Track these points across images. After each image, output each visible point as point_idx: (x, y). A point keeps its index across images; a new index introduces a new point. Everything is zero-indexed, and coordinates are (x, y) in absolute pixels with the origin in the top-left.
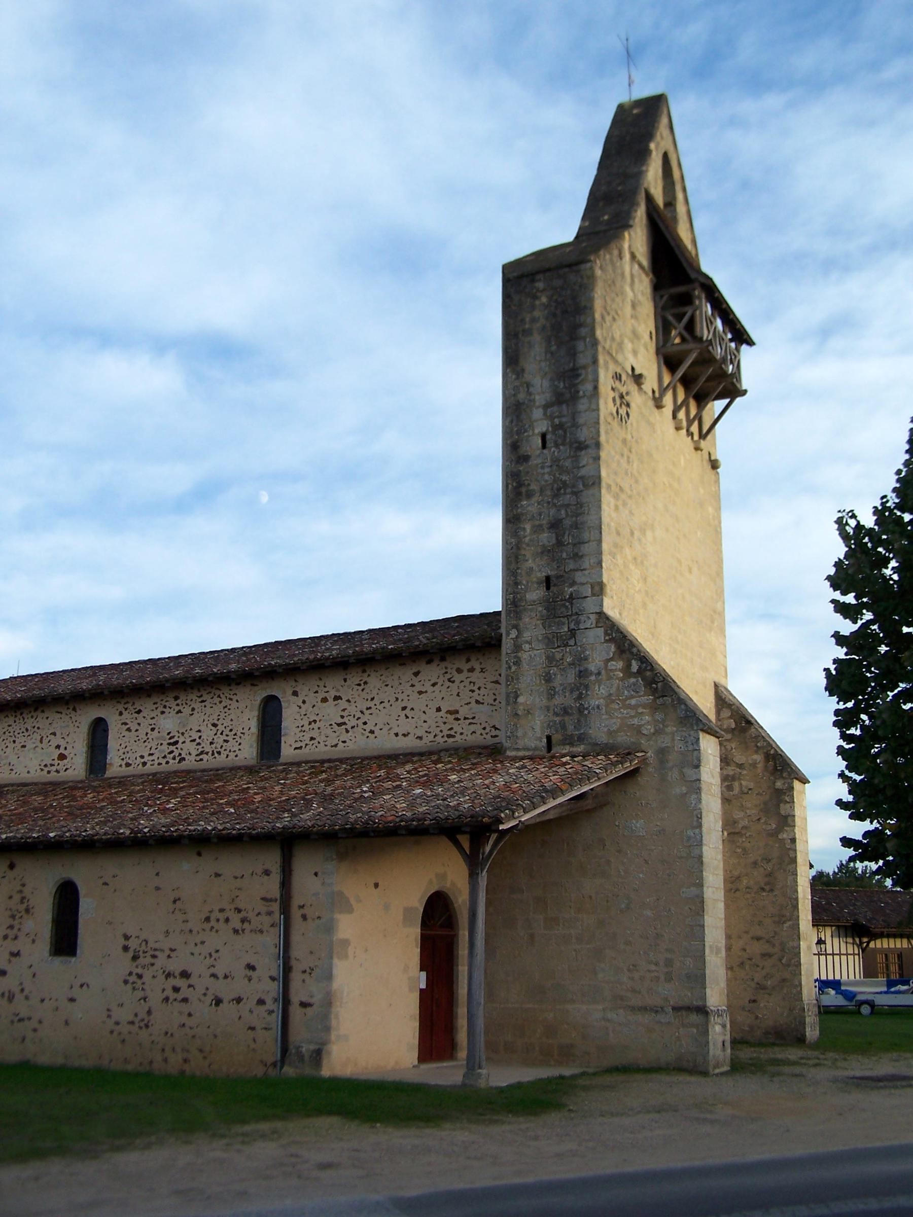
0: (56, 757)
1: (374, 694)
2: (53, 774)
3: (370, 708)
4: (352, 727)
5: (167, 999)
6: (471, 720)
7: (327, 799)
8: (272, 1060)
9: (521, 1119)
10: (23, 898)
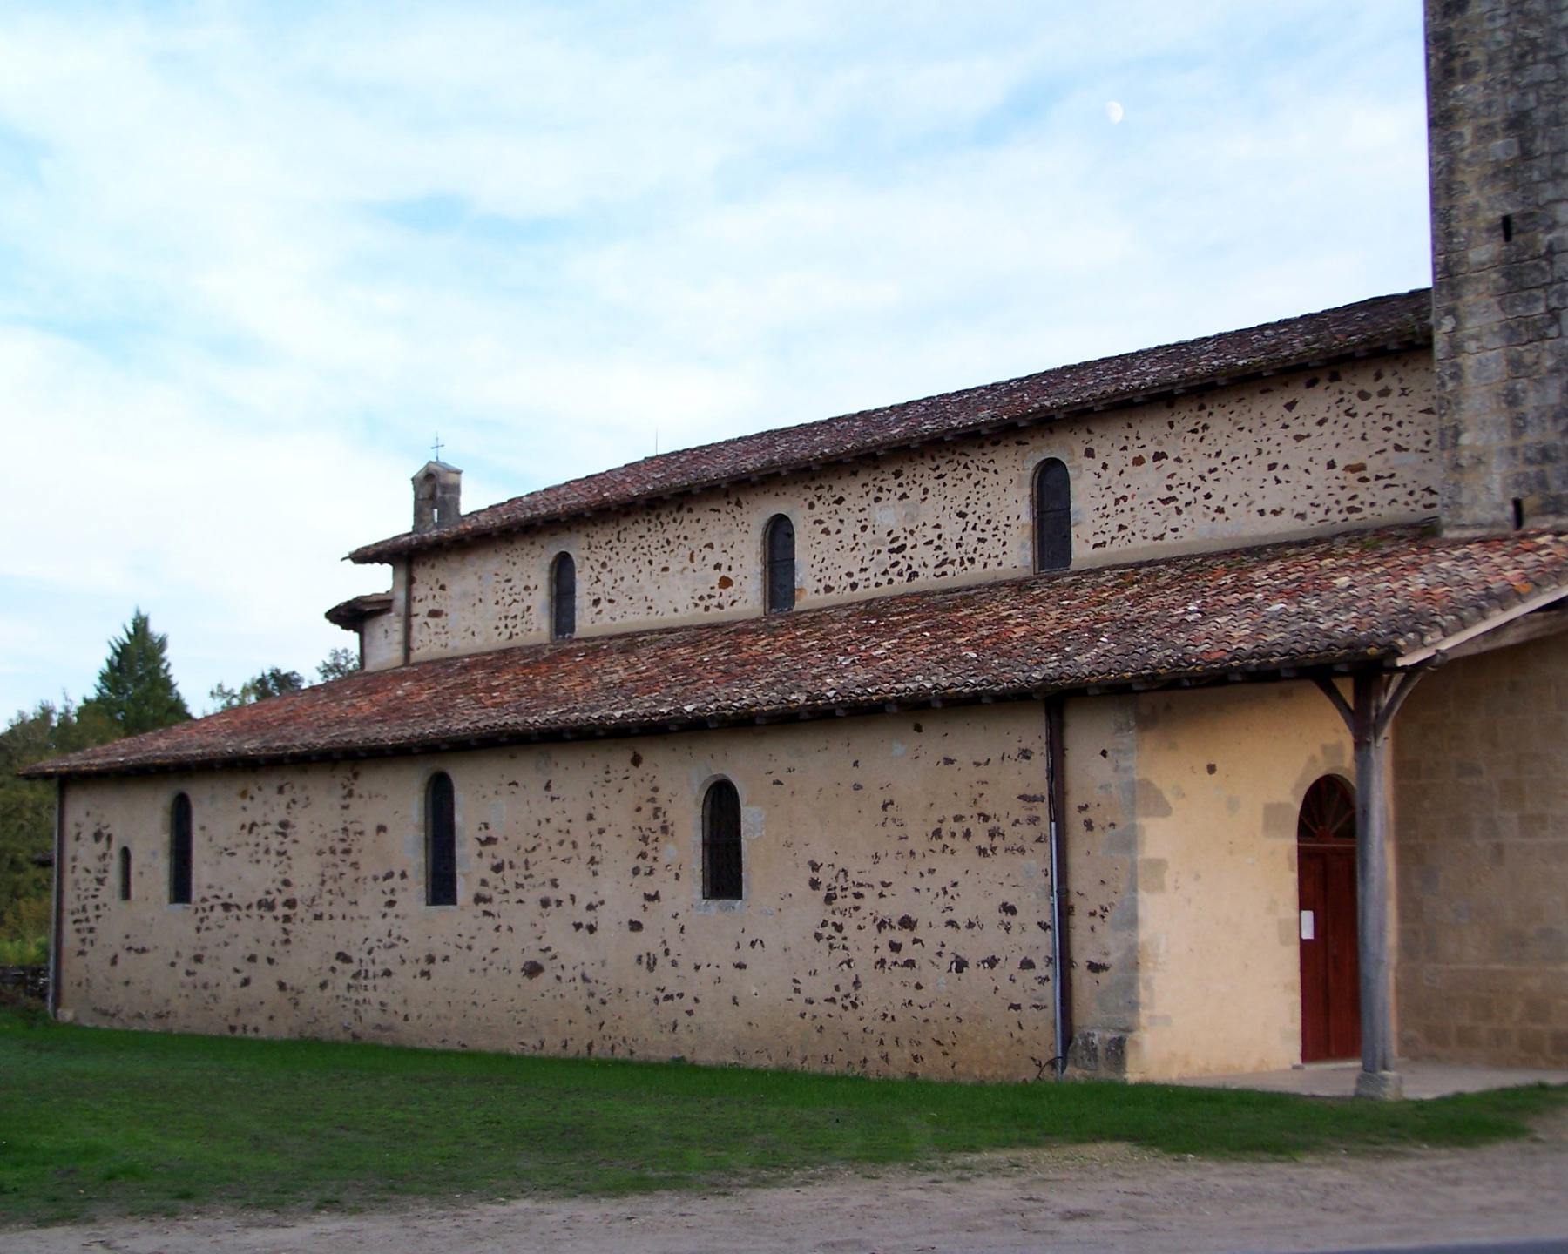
0: (716, 582)
1: (1220, 446)
2: (714, 610)
3: (1216, 469)
4: (1187, 504)
5: (882, 962)
6: (1388, 479)
7: (1129, 626)
8: (1051, 1056)
9: (1444, 1152)
10: (657, 809)
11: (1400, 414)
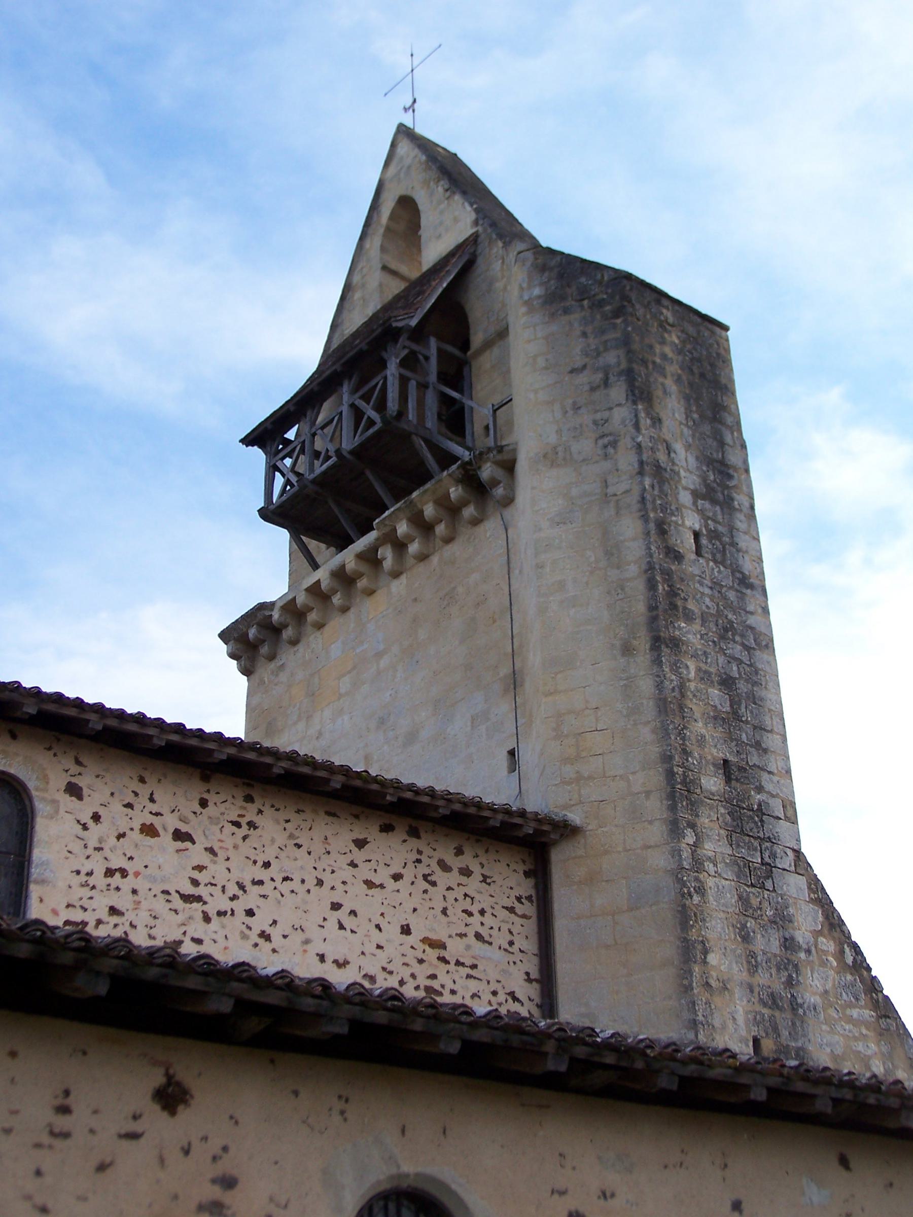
1: (269, 856)
4: (221, 914)
11: (483, 901)
